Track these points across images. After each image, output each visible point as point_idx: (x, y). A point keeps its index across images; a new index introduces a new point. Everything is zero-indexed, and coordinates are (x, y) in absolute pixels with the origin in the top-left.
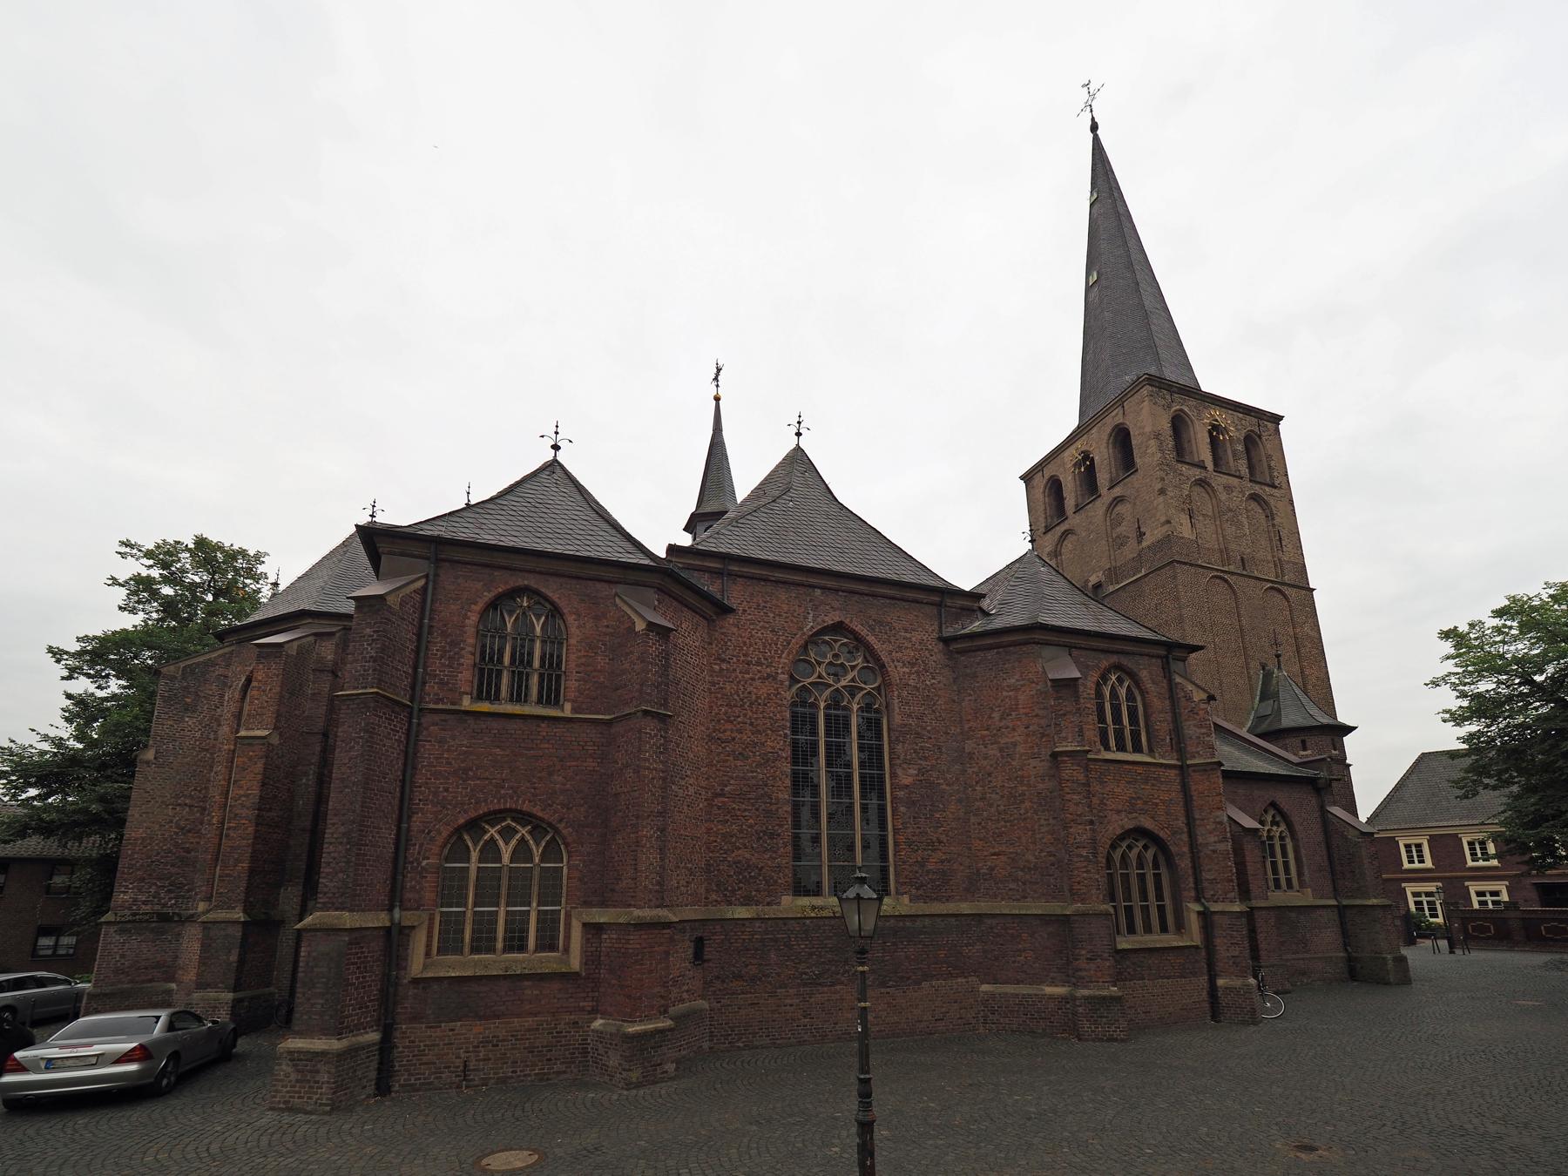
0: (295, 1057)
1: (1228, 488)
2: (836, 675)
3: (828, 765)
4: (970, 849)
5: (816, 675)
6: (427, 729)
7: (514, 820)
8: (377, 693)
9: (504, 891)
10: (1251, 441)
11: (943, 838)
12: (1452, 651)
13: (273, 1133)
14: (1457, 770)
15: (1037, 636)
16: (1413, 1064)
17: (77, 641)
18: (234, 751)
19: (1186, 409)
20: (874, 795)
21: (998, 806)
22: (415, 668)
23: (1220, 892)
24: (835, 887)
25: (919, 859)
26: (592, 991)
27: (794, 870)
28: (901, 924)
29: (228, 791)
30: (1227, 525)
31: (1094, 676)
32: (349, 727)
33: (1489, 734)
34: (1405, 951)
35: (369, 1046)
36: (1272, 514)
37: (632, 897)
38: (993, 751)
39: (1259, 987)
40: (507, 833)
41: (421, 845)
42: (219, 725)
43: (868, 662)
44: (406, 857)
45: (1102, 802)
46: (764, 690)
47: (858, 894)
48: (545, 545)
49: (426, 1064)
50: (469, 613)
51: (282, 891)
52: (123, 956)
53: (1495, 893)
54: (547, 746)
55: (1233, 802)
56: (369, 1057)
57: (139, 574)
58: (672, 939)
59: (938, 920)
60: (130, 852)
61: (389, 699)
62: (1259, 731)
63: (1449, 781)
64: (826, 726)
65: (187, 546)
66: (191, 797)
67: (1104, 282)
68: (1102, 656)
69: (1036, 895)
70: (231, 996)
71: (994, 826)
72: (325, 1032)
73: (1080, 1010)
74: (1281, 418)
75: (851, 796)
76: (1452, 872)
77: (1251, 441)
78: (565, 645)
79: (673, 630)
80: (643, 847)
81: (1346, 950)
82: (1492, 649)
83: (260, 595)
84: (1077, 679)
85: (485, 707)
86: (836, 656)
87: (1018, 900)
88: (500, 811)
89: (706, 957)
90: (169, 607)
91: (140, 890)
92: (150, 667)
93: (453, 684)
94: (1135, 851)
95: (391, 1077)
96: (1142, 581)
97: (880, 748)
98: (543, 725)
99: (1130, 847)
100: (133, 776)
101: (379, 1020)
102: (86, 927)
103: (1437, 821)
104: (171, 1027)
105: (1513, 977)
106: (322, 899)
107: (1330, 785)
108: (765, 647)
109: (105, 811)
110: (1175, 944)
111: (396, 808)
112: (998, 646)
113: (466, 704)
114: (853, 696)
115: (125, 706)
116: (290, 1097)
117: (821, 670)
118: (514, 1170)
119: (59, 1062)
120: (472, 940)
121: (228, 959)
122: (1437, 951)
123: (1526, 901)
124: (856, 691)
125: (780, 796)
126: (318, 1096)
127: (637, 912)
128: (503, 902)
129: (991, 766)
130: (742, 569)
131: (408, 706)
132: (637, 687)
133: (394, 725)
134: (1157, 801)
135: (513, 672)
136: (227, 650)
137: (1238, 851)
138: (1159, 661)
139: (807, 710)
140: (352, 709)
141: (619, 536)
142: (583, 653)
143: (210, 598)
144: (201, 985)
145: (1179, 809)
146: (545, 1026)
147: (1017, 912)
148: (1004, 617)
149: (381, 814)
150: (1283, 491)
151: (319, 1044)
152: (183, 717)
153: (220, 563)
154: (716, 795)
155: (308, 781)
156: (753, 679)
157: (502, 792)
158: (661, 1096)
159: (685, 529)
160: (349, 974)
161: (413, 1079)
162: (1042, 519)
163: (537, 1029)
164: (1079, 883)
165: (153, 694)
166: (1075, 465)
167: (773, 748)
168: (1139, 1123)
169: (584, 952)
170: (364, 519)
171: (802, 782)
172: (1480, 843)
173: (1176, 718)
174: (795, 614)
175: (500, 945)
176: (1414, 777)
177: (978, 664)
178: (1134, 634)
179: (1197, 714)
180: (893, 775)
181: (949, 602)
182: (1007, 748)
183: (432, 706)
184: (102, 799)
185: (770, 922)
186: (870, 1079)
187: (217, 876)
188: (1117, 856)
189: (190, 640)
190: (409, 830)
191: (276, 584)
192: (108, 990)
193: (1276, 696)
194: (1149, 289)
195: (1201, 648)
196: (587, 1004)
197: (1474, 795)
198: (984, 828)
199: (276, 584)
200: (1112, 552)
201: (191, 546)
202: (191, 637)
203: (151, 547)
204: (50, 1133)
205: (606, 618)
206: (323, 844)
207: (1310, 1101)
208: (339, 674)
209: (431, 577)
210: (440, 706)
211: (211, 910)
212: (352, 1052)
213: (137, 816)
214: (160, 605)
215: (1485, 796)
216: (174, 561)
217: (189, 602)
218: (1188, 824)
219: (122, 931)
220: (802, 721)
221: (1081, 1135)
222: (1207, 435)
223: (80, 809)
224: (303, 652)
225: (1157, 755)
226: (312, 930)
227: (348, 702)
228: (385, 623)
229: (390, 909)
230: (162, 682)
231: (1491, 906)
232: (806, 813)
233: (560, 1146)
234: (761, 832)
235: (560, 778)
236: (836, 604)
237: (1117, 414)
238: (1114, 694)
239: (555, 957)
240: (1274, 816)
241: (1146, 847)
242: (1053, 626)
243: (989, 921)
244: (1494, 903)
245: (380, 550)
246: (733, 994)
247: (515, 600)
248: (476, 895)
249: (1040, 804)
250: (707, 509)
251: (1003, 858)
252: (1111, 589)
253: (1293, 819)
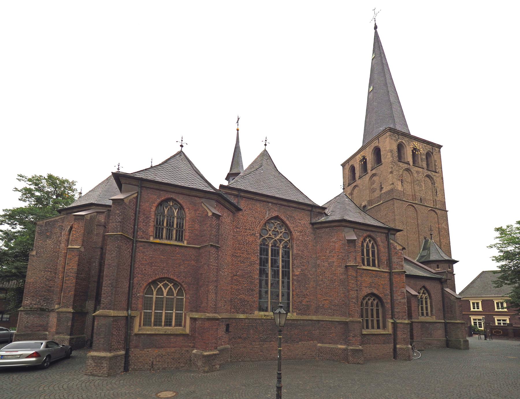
0: (94, 358)
1: (418, 172)
2: (275, 235)
3: (272, 266)
4: (317, 298)
5: (269, 234)
6: (138, 248)
7: (167, 281)
8: (121, 234)
9: (164, 306)
10: (428, 155)
11: (308, 294)
12: (499, 235)
13: (86, 383)
14: (495, 278)
15: (344, 224)
16: (466, 376)
17: (3, 211)
18: (67, 253)
19: (404, 142)
20: (286, 278)
21: (327, 283)
22: (134, 226)
23: (401, 316)
24: (272, 309)
25: (300, 300)
26: (193, 341)
27: (259, 303)
28: (293, 322)
29: (65, 267)
30: (416, 186)
31: (361, 239)
32: (111, 246)
33: (509, 265)
34: (468, 338)
35: (121, 355)
36: (434, 182)
37: (206, 309)
38: (326, 264)
39: (412, 349)
40: (165, 286)
41: (137, 288)
42: (60, 243)
43: (286, 230)
44: (132, 292)
45: (361, 284)
46: (251, 239)
47: (280, 312)
48: (178, 183)
49: (139, 362)
50: (152, 207)
51: (87, 302)
52: (27, 322)
53: (505, 320)
54: (178, 256)
55: (409, 285)
56: (121, 359)
57: (26, 187)
58: (219, 324)
59: (305, 321)
60: (28, 287)
61: (126, 237)
62: (421, 261)
63: (492, 281)
64: (271, 253)
65: (44, 177)
66: (51, 268)
67: (374, 91)
68: (364, 232)
69: (337, 314)
70: (69, 337)
71: (325, 290)
72: (105, 350)
73: (349, 353)
74: (442, 146)
75: (279, 278)
76: (489, 312)
77: (428, 155)
78: (185, 220)
79: (221, 216)
80: (210, 292)
81: (446, 337)
82: (515, 235)
83: (74, 197)
84: (355, 240)
85: (158, 241)
86: (275, 228)
87: (331, 316)
88: (163, 278)
89: (230, 331)
90: (39, 200)
91: (33, 300)
92: (32, 222)
93: (147, 232)
94: (370, 301)
95: (129, 366)
96: (381, 205)
97: (289, 261)
98: (177, 248)
99: (369, 300)
100: (28, 260)
101: (124, 347)
102: (13, 312)
103: (485, 295)
104: (47, 346)
105: (507, 349)
106: (102, 306)
107: (446, 281)
108: (252, 223)
109: (18, 272)
110: (382, 333)
111: (129, 275)
113: (152, 239)
114: (281, 242)
115: (23, 235)
116: (93, 371)
117: (270, 233)
118: (168, 397)
119: (6, 357)
120: (154, 322)
121: (67, 325)
122: (480, 339)
123: (515, 323)
124: (282, 241)
125: (255, 277)
126: (103, 371)
127: (208, 315)
128: (164, 309)
129: (325, 269)
130: (245, 195)
131: (132, 239)
132: (209, 236)
133: (128, 246)
134: (380, 284)
135: (167, 229)
136: (62, 216)
137: (409, 302)
138: (385, 235)
139: (265, 247)
140: (112, 240)
141: (203, 180)
142: (190, 223)
143: (55, 197)
144: (57, 333)
145: (388, 288)
146: (178, 351)
147: (331, 320)
148: (333, 217)
149: (124, 277)
150: (439, 174)
151: (103, 354)
152: (46, 240)
153: (58, 184)
154: (234, 276)
155: (96, 264)
156: (247, 235)
157: (164, 271)
158: (214, 376)
159: (226, 179)
160: (113, 331)
161: (136, 367)
162: (347, 181)
163: (175, 352)
164: (351, 311)
165: (34, 231)
166: (360, 161)
167: (253, 260)
168: (365, 391)
169: (190, 327)
170: (115, 170)
171: (263, 272)
172: (501, 303)
173: (389, 255)
174: (262, 212)
175: (163, 324)
176: (479, 279)
177: (323, 233)
178: (376, 225)
179: (398, 254)
180: (293, 271)
181: (314, 210)
183: (140, 240)
184: (16, 268)
185: (251, 320)
186: (281, 373)
187: (62, 296)
188: (364, 302)
189: (48, 212)
190: (133, 283)
191: (81, 193)
192: (23, 333)
193: (429, 249)
194: (393, 94)
195: (401, 230)
196: (191, 345)
197: (501, 287)
198: (322, 291)
199: (81, 193)
200: (370, 194)
201: (46, 177)
202: (48, 211)
203: (30, 177)
204: (4, 379)
205: (198, 211)
206: (102, 286)
207: (427, 386)
208: (107, 227)
209: (139, 193)
210: (143, 240)
211: (60, 308)
212: (115, 357)
213: (30, 274)
214: (35, 199)
215: (505, 287)
216: (40, 183)
217: (47, 198)
218: (391, 292)
219: (27, 314)
220: (263, 251)
221: (347, 394)
222: (411, 152)
223: (8, 271)
224: (92, 219)
225: (381, 268)
226: (99, 316)
227: (110, 237)
228: (124, 209)
229: (127, 310)
230: (37, 227)
231: (502, 325)
232: (263, 283)
233: (182, 390)
234: (249, 289)
235: (183, 267)
236: (276, 209)
237: (376, 142)
238: (367, 246)
239: (181, 329)
240: (424, 291)
241: (374, 300)
242: (349, 220)
243: (321, 323)
244: (503, 323)
245: (122, 182)
246: (238, 343)
247: (168, 203)
248: (155, 307)
249: (341, 284)
250: (231, 172)
251: (327, 301)
252: (369, 208)
253: (431, 292)
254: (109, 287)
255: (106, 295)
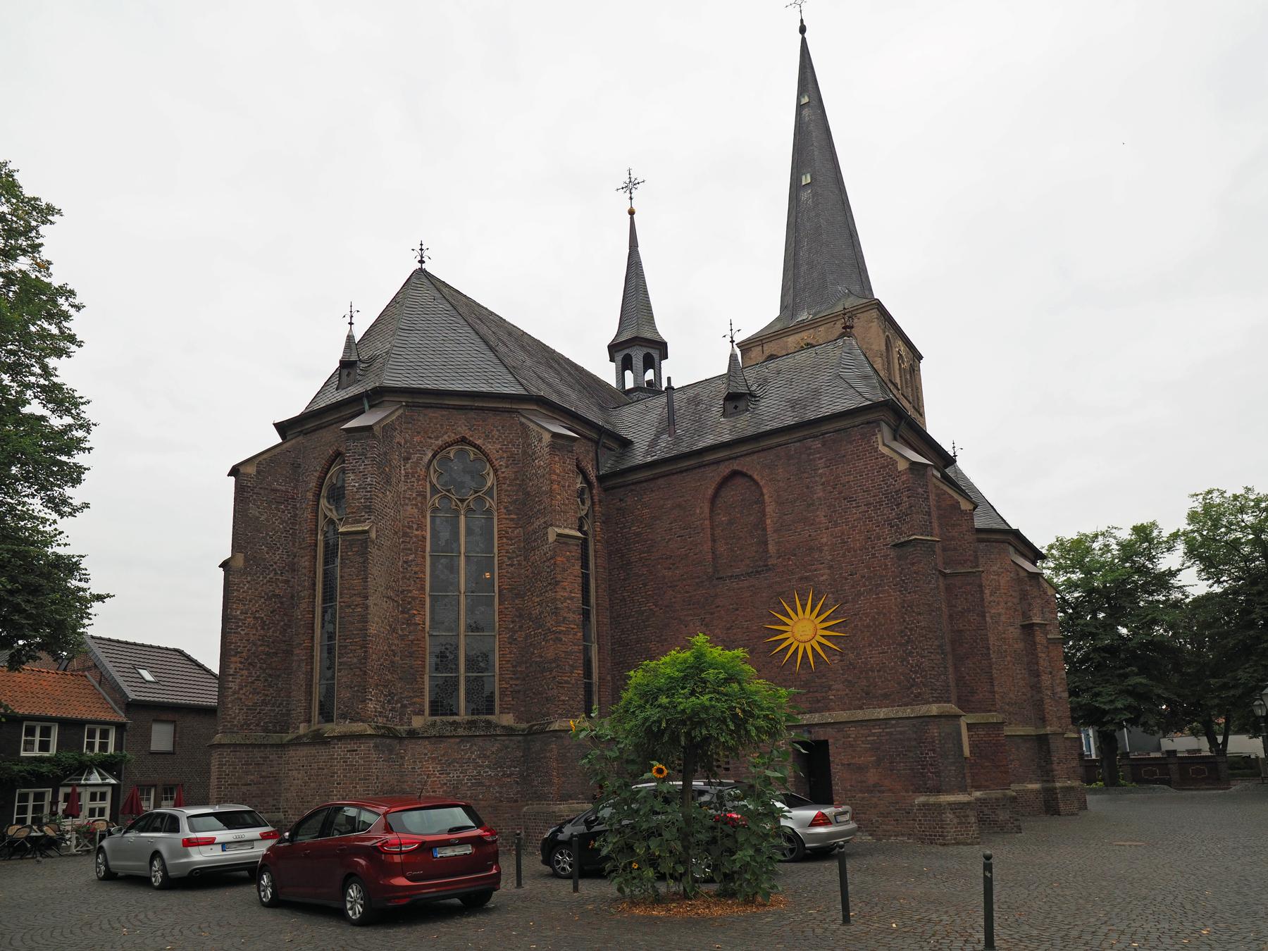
112: (988, 541)
182: (995, 617)
254: (938, 653)
255: (937, 671)
